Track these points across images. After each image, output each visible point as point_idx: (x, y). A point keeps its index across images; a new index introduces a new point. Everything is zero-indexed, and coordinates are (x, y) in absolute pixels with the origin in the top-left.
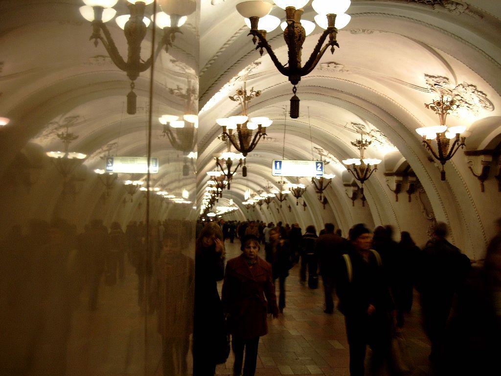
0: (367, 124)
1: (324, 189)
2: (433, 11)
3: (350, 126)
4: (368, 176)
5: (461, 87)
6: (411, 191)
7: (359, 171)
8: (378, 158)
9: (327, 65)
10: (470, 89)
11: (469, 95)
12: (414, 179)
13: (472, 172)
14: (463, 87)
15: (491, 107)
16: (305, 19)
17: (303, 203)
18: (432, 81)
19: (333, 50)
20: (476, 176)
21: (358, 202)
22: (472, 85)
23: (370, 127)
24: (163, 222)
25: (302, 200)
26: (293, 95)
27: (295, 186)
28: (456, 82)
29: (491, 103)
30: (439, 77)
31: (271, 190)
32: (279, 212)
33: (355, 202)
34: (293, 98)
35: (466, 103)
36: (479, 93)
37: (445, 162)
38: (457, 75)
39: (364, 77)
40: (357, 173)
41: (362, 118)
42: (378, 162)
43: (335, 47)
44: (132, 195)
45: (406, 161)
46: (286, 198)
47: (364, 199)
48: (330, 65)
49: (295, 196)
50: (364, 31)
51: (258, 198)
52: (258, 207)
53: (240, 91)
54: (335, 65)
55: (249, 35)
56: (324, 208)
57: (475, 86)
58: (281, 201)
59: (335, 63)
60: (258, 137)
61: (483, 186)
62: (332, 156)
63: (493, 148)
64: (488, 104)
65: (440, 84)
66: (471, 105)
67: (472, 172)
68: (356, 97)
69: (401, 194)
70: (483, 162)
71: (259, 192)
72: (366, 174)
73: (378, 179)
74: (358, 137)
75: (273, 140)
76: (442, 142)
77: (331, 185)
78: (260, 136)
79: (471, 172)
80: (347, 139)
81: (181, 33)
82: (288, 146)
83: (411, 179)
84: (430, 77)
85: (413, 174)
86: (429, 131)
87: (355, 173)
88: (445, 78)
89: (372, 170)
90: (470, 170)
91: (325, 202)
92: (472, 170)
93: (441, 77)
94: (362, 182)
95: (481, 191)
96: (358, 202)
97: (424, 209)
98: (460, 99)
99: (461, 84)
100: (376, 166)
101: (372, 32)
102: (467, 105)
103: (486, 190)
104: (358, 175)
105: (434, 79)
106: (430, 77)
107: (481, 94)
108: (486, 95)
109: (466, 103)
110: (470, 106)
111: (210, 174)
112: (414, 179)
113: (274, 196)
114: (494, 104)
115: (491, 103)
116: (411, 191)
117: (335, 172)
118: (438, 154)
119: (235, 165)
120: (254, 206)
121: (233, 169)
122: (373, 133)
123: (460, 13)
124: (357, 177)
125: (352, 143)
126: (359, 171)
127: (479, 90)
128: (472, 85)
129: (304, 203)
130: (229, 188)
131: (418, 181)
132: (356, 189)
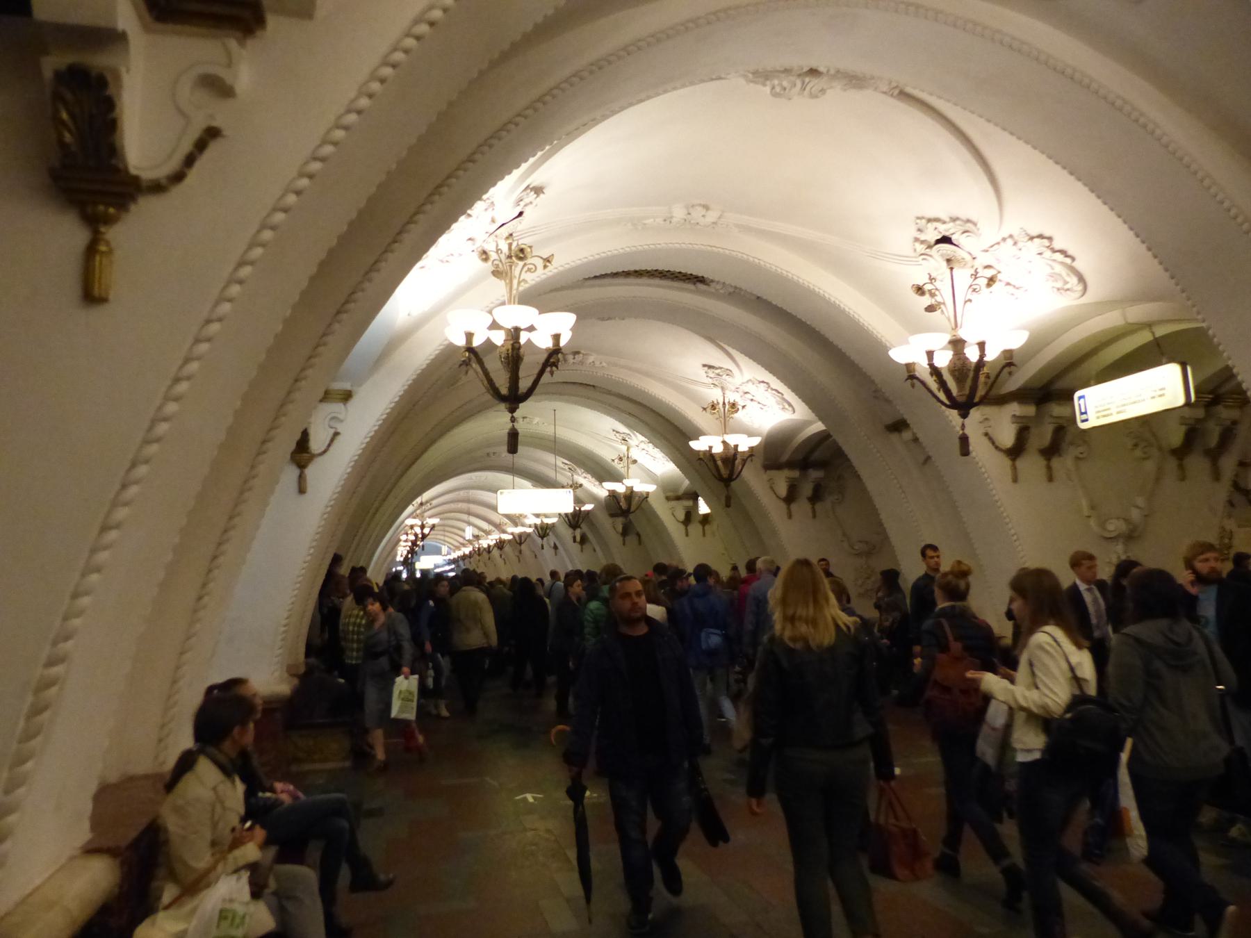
0: (634, 434)
1: (632, 512)
5: (1010, 242)
7: (540, 530)
11: (760, 392)
13: (775, 494)
15: (790, 409)
17: (552, 545)
19: (552, 373)
22: (763, 382)
24: (104, 233)
25: (551, 539)
27: (602, 491)
29: (790, 405)
30: (624, 433)
32: (505, 563)
36: (774, 392)
37: (968, 413)
43: (554, 368)
45: (822, 438)
47: (638, 535)
48: (691, 210)
49: (540, 536)
57: (767, 383)
61: (624, 541)
64: (787, 406)
67: (775, 494)
75: (712, 216)
76: (731, 458)
77: (647, 501)
80: (607, 453)
81: (302, 490)
86: (708, 443)
88: (968, 221)
95: (1011, 480)
96: (631, 539)
97: (1093, 508)
98: (752, 398)
99: (750, 380)
102: (760, 406)
103: (689, 534)
107: (776, 394)
108: (782, 394)
109: (759, 403)
111: (409, 522)
113: (510, 537)
114: (794, 406)
115: (790, 405)
116: (1051, 451)
117: (652, 477)
120: (489, 550)
122: (750, 387)
126: (540, 530)
127: (774, 388)
128: (763, 382)
129: (555, 544)
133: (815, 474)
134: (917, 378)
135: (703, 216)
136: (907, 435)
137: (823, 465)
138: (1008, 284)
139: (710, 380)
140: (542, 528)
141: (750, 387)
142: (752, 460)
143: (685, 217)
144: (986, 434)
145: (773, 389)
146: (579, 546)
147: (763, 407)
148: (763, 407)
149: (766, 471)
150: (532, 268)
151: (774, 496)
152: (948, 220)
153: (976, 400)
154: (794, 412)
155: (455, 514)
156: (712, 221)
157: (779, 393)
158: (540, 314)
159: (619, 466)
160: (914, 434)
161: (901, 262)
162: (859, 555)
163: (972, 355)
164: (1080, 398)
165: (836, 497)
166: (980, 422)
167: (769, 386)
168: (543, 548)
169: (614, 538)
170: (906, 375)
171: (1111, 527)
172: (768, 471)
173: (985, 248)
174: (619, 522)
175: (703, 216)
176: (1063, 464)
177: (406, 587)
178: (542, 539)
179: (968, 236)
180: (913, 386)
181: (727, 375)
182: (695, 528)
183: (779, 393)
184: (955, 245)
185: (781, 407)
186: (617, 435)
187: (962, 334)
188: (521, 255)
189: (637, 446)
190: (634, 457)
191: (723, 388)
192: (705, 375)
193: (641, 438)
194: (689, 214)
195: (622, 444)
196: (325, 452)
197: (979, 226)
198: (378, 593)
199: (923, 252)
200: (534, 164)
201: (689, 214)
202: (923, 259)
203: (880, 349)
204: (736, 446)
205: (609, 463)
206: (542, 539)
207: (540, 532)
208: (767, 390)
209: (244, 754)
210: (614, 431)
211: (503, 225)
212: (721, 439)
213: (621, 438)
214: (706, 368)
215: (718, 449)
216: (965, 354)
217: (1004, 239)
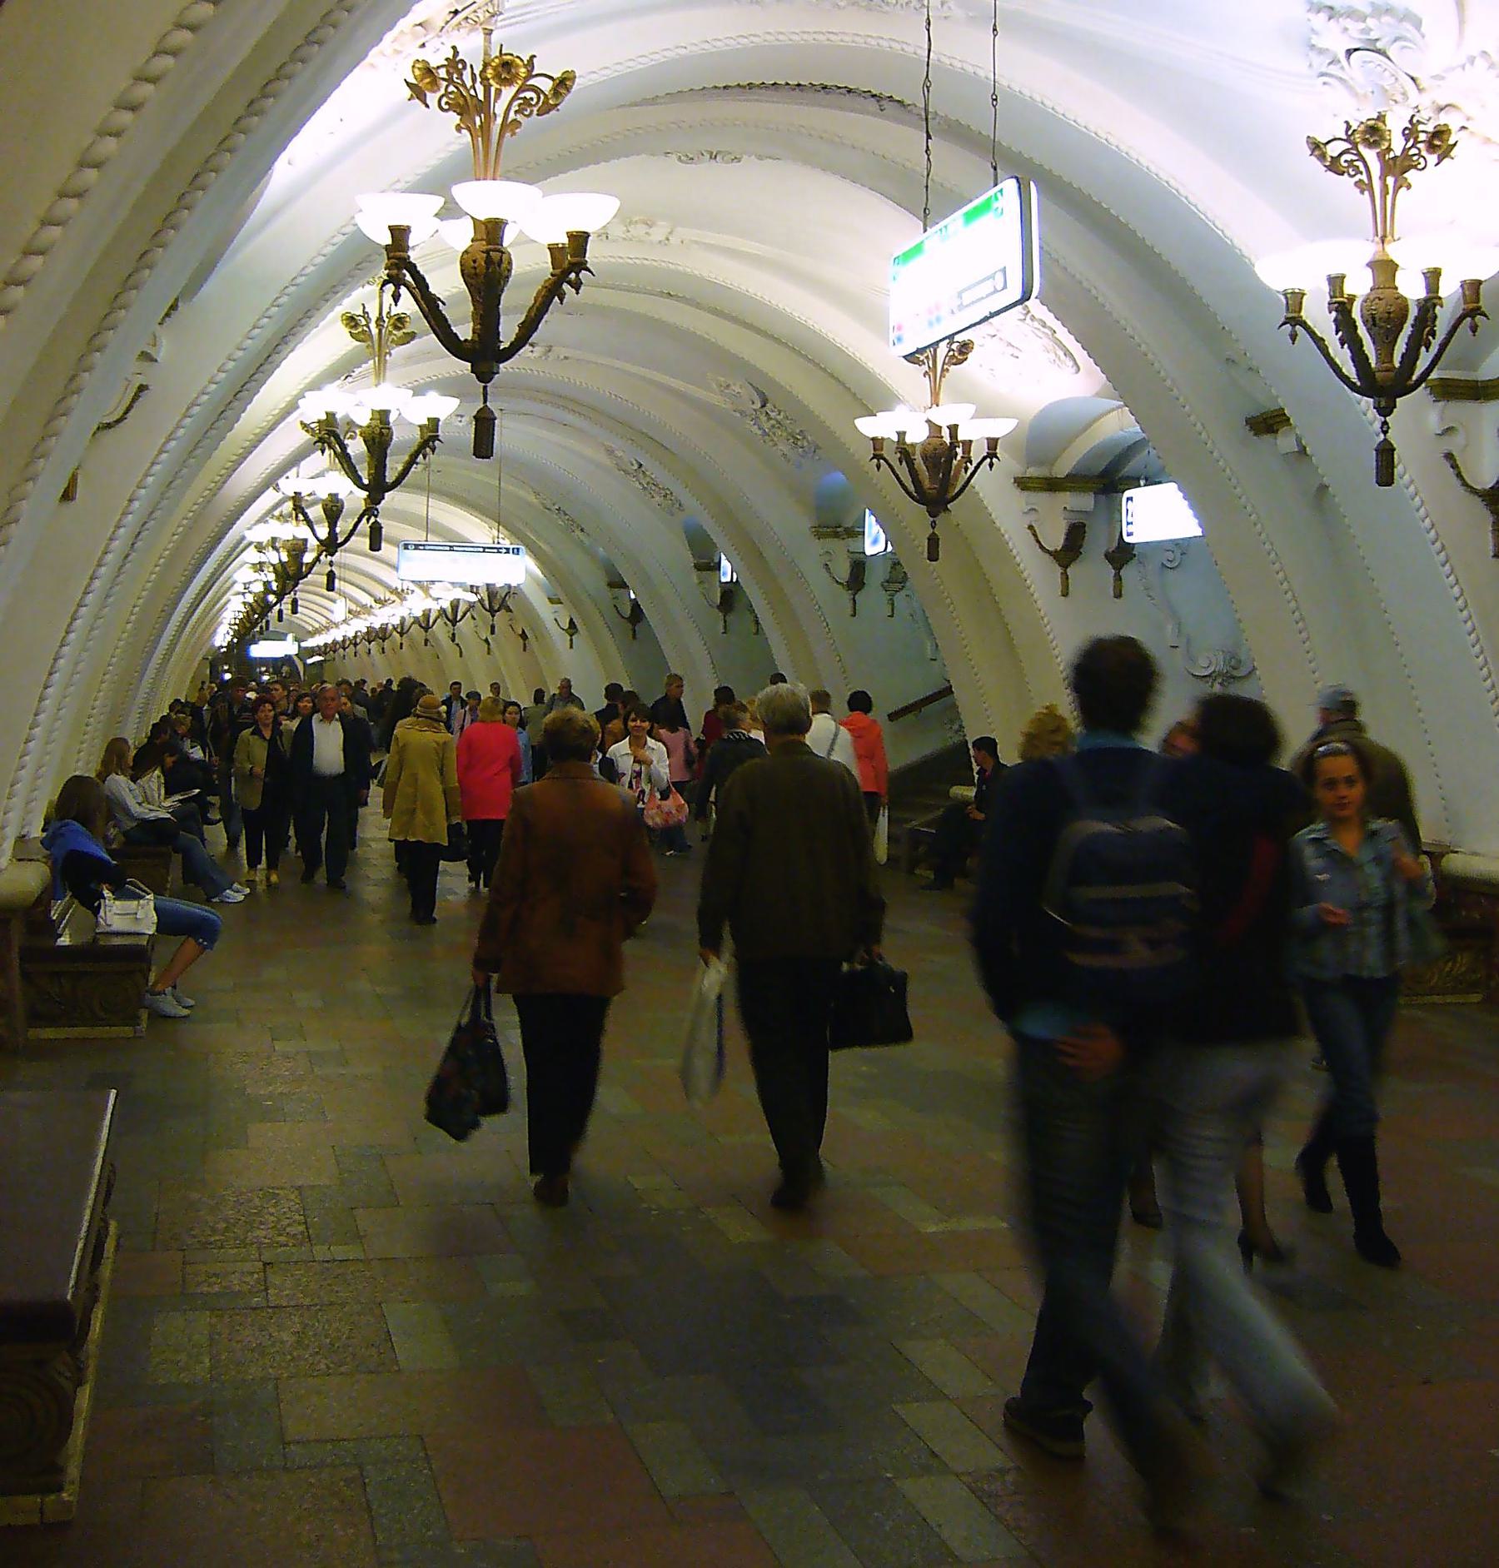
13: (1459, 475)
16: (362, 453)
20: (1473, 491)
26: (1382, 436)
29: (1067, 353)
36: (1036, 324)
39: (750, 251)
42: (1000, 428)
44: (1385, 410)
46: (509, 603)
49: (920, 496)
50: (713, 157)
51: (359, 625)
52: (440, 630)
53: (507, 65)
58: (492, 612)
67: (1459, 475)
68: (715, 312)
71: (367, 610)
82: (347, 577)
92: (1454, 466)
100: (993, 443)
101: (737, 159)
102: (1011, 350)
104: (1359, 358)
115: (1067, 353)
118: (487, 606)
119: (350, 515)
121: (343, 527)
124: (912, 488)
125: (1316, 147)
129: (523, 631)
130: (483, 445)
134: (1304, 325)
135: (647, 233)
136: (1285, 442)
140: (1387, 320)
144: (1031, 527)
145: (1033, 318)
148: (1017, 353)
150: (532, 99)
151: (1458, 482)
152: (1367, 10)
153: (459, 618)
155: (318, 597)
158: (413, 395)
160: (1299, 440)
161: (466, 549)
163: (1412, 288)
164: (1128, 499)
167: (1029, 312)
168: (1385, 475)
170: (1282, 315)
175: (647, 233)
177: (220, 669)
180: (1293, 337)
182: (1092, 570)
184: (1388, 58)
187: (1393, 251)
188: (400, 325)
190: (916, 371)
196: (118, 421)
199: (1324, 70)
203: (1235, 267)
204: (901, 435)
207: (927, 484)
215: (917, 435)
216: (1396, 288)
217: (1472, 60)
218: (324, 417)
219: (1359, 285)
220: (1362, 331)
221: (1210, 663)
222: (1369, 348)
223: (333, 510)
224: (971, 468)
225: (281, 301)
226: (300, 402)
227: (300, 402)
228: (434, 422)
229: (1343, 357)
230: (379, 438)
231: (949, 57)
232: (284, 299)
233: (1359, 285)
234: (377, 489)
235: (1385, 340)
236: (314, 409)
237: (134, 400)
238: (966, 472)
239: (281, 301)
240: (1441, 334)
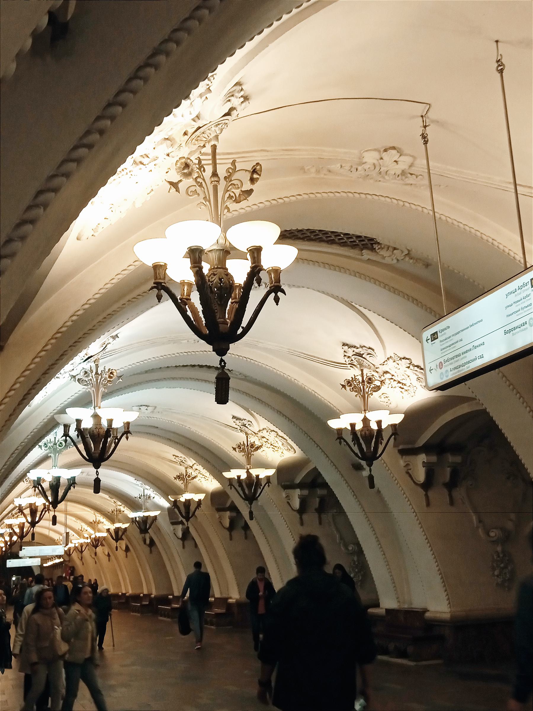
1: (149, 528)
2: (360, 257)
3: (231, 422)
4: (380, 452)
6: (321, 510)
8: (272, 468)
9: (376, 155)
10: (405, 363)
12: (323, 492)
13: (412, 479)
14: (394, 361)
15: (292, 450)
17: (124, 548)
18: (350, 352)
20: (294, 511)
21: (238, 534)
23: (191, 461)
25: (123, 544)
28: (385, 352)
29: (292, 447)
31: (100, 526)
32: (96, 563)
33: (127, 553)
34: (56, 508)
35: (399, 382)
36: (416, 368)
38: (386, 344)
40: (243, 490)
41: (247, 410)
42: (271, 472)
54: (146, 408)
55: (41, 449)
56: (231, 539)
59: (146, 406)
60: (43, 513)
61: (231, 536)
62: (200, 468)
63: (309, 480)
65: (246, 426)
66: (275, 447)
67: (412, 479)
69: (153, 547)
70: (300, 497)
72: (256, 491)
73: (166, 528)
74: (241, 437)
78: (45, 512)
79: (409, 479)
83: (320, 492)
84: (350, 347)
85: (325, 485)
87: (239, 489)
88: (370, 348)
89: (263, 485)
90: (407, 475)
91: (152, 544)
92: (176, 535)
93: (364, 346)
94: (96, 549)
95: (229, 539)
96: (238, 534)
97: (480, 521)
98: (391, 377)
100: (126, 528)
102: (400, 385)
103: (128, 557)
105: (355, 349)
106: (350, 347)
107: (418, 369)
110: (404, 387)
112: (323, 492)
116: (321, 510)
117: (157, 507)
123: (398, 260)
127: (281, 435)
131: (331, 493)
132: (234, 514)
133: (452, 459)
135: (146, 409)
137: (457, 449)
138: (399, 382)
139: (347, 360)
141: (390, 366)
142: (269, 486)
143: (376, 162)
146: (148, 549)
147: (205, 477)
149: (284, 490)
152: (359, 347)
154: (295, 452)
156: (150, 411)
157: (284, 439)
159: (179, 483)
162: (495, 542)
165: (335, 511)
166: (404, 466)
169: (175, 545)
170: (336, 436)
171: (492, 534)
172: (404, 457)
173: (382, 363)
174: (179, 529)
176: (459, 493)
178: (117, 542)
179: (370, 356)
181: (249, 425)
183: (284, 439)
185: (286, 448)
186: (238, 422)
189: (192, 467)
191: (246, 434)
192: (342, 354)
193: (264, 423)
194: (382, 159)
195: (181, 465)
197: (375, 351)
198: (367, 611)
199: (349, 362)
200: (261, 42)
201: (382, 159)
202: (350, 366)
205: (172, 482)
206: (117, 542)
208: (409, 367)
209: (257, 263)
210: (173, 455)
211: (205, 125)
212: (362, 416)
213: (240, 424)
214: (235, 420)
218: (36, 479)
219: (359, 426)
220: (361, 441)
221: (496, 535)
222: (364, 446)
223: (33, 511)
224: (262, 487)
225: (46, 348)
226: (27, 474)
227: (27, 474)
228: (200, 500)
229: (356, 449)
230: (55, 485)
231: (458, 222)
232: (49, 347)
233: (359, 426)
234: (55, 503)
235: (368, 444)
236: (33, 475)
237: (242, 162)
238: (260, 489)
239: (46, 348)
240: (384, 442)
